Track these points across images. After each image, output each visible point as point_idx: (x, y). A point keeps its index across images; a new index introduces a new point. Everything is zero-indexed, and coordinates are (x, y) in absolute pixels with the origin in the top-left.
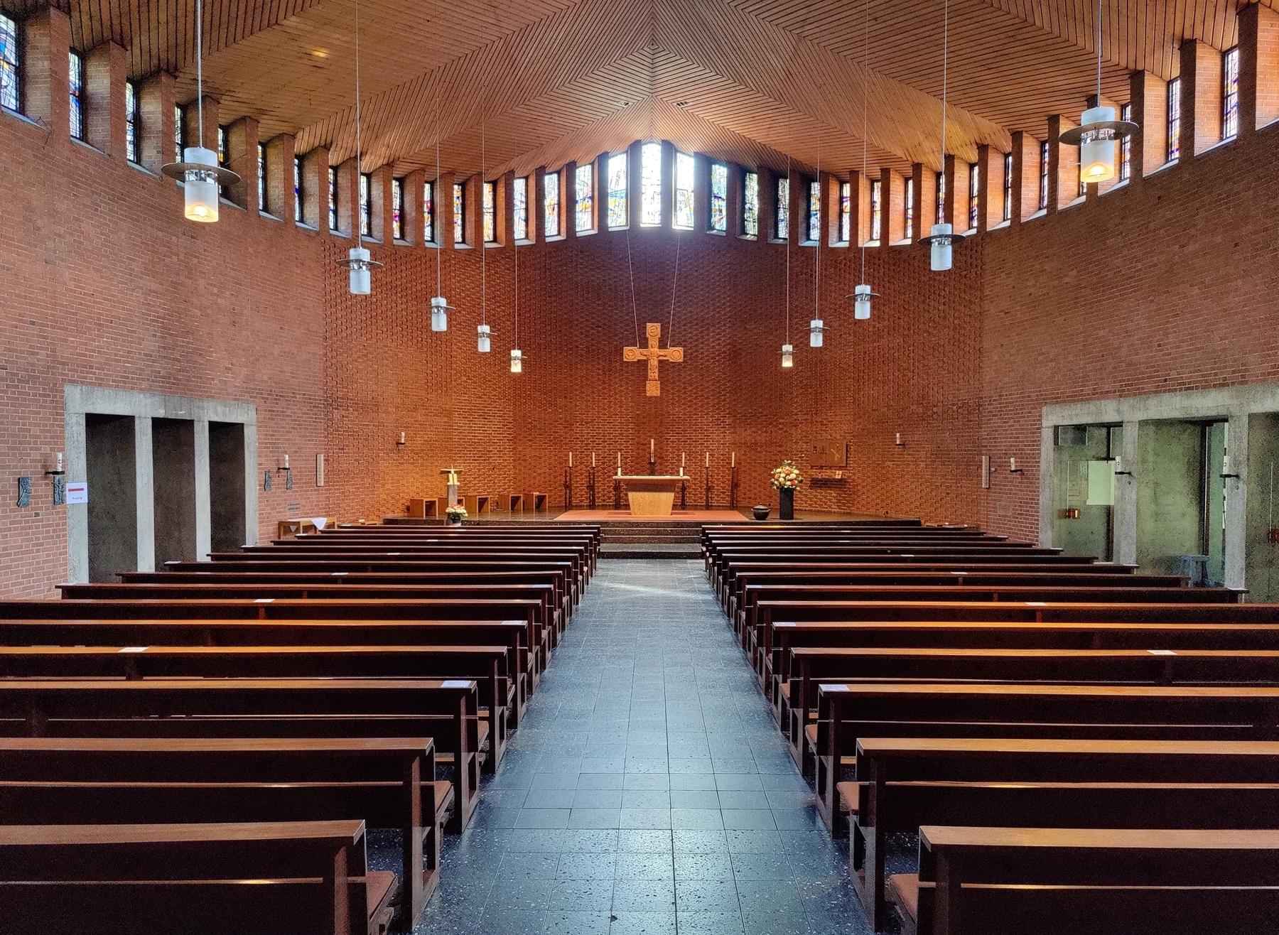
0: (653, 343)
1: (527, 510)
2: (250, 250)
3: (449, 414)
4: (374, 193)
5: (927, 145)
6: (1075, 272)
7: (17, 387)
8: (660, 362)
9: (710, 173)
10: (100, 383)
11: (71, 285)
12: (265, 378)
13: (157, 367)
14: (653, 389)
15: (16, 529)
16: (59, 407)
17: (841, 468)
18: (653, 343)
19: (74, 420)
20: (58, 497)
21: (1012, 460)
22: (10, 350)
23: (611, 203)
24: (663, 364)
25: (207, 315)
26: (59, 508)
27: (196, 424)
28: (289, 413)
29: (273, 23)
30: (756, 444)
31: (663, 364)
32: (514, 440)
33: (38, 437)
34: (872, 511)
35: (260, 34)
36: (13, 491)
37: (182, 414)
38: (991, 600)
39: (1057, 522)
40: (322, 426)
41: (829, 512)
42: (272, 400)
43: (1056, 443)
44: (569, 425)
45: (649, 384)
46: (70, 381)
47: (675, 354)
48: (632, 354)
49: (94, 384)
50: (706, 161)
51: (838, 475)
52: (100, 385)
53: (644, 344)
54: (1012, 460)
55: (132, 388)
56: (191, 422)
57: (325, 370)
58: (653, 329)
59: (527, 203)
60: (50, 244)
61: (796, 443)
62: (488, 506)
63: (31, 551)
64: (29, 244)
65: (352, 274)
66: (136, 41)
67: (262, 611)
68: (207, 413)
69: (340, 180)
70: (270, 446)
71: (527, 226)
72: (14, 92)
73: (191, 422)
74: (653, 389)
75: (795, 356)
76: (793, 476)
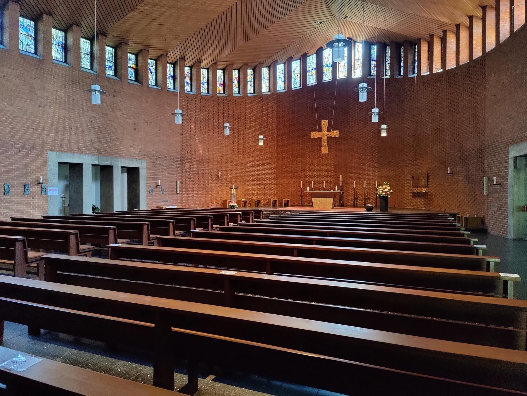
0: (325, 129)
1: (281, 206)
2: (144, 100)
3: (245, 165)
4: (210, 75)
5: (457, 13)
6: (521, 66)
7: (24, 151)
8: (328, 137)
9: (370, 49)
10: (66, 151)
11: (52, 115)
12: (151, 150)
13: (95, 145)
14: (325, 150)
15: (22, 203)
16: (46, 159)
17: (425, 187)
18: (325, 129)
19: (52, 164)
20: (44, 191)
21: (494, 178)
22: (21, 138)
23: (325, 70)
24: (330, 139)
25: (121, 126)
26: (44, 196)
27: (114, 167)
28: (163, 164)
29: (133, 9)
30: (389, 176)
31: (330, 139)
32: (277, 176)
33: (34, 170)
34: (439, 209)
35: (130, 13)
36: (22, 189)
37: (108, 163)
38: (32, 227)
39: (516, 214)
40: (179, 169)
41: (421, 210)
42: (155, 160)
43: (515, 167)
44: (303, 170)
45: (323, 148)
46: (51, 150)
47: (335, 134)
48: (315, 135)
49: (63, 151)
50: (368, 45)
51: (424, 190)
52: (66, 152)
53: (321, 130)
54: (494, 178)
55: (82, 153)
56: (112, 167)
57: (182, 147)
58: (325, 123)
59: (285, 74)
60: (42, 100)
61: (406, 175)
62: (261, 204)
63: (30, 212)
64: (31, 100)
65: (92, 96)
66: (83, 23)
67: (295, 251)
68: (119, 163)
69: (193, 72)
70: (152, 176)
71: (285, 84)
72: (33, 47)
73: (112, 167)
74: (325, 150)
75: (388, 131)
76: (387, 190)
